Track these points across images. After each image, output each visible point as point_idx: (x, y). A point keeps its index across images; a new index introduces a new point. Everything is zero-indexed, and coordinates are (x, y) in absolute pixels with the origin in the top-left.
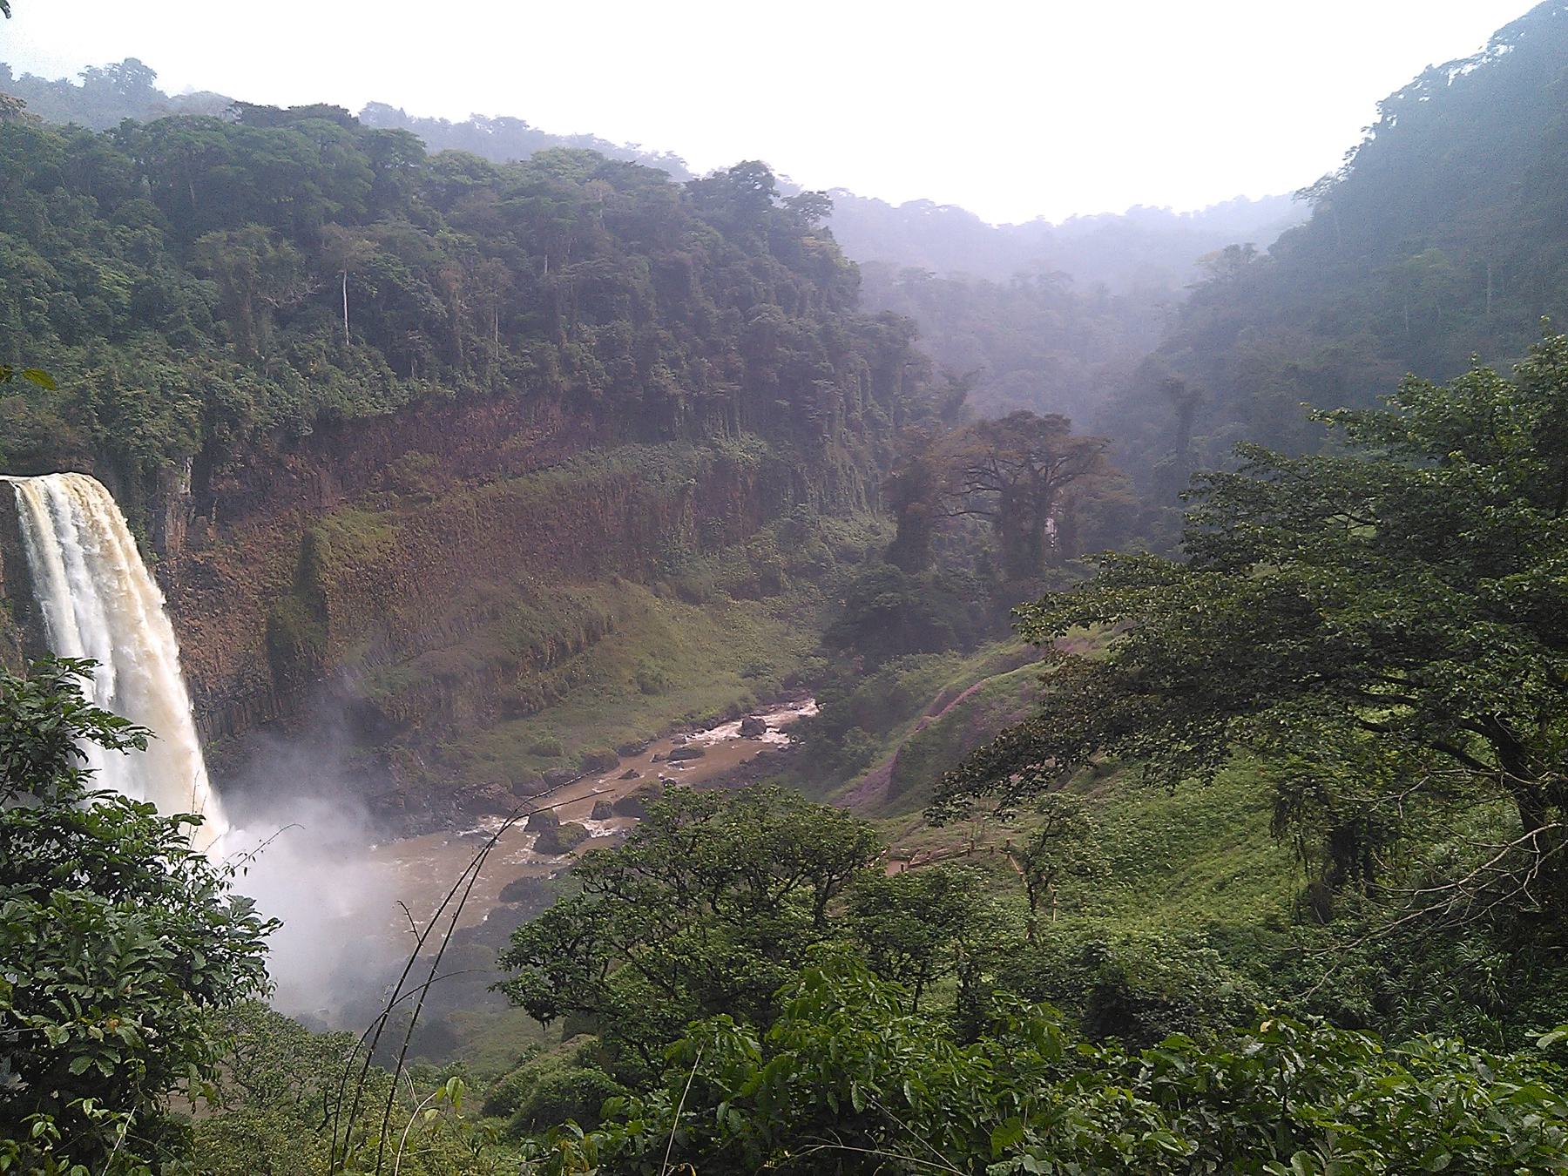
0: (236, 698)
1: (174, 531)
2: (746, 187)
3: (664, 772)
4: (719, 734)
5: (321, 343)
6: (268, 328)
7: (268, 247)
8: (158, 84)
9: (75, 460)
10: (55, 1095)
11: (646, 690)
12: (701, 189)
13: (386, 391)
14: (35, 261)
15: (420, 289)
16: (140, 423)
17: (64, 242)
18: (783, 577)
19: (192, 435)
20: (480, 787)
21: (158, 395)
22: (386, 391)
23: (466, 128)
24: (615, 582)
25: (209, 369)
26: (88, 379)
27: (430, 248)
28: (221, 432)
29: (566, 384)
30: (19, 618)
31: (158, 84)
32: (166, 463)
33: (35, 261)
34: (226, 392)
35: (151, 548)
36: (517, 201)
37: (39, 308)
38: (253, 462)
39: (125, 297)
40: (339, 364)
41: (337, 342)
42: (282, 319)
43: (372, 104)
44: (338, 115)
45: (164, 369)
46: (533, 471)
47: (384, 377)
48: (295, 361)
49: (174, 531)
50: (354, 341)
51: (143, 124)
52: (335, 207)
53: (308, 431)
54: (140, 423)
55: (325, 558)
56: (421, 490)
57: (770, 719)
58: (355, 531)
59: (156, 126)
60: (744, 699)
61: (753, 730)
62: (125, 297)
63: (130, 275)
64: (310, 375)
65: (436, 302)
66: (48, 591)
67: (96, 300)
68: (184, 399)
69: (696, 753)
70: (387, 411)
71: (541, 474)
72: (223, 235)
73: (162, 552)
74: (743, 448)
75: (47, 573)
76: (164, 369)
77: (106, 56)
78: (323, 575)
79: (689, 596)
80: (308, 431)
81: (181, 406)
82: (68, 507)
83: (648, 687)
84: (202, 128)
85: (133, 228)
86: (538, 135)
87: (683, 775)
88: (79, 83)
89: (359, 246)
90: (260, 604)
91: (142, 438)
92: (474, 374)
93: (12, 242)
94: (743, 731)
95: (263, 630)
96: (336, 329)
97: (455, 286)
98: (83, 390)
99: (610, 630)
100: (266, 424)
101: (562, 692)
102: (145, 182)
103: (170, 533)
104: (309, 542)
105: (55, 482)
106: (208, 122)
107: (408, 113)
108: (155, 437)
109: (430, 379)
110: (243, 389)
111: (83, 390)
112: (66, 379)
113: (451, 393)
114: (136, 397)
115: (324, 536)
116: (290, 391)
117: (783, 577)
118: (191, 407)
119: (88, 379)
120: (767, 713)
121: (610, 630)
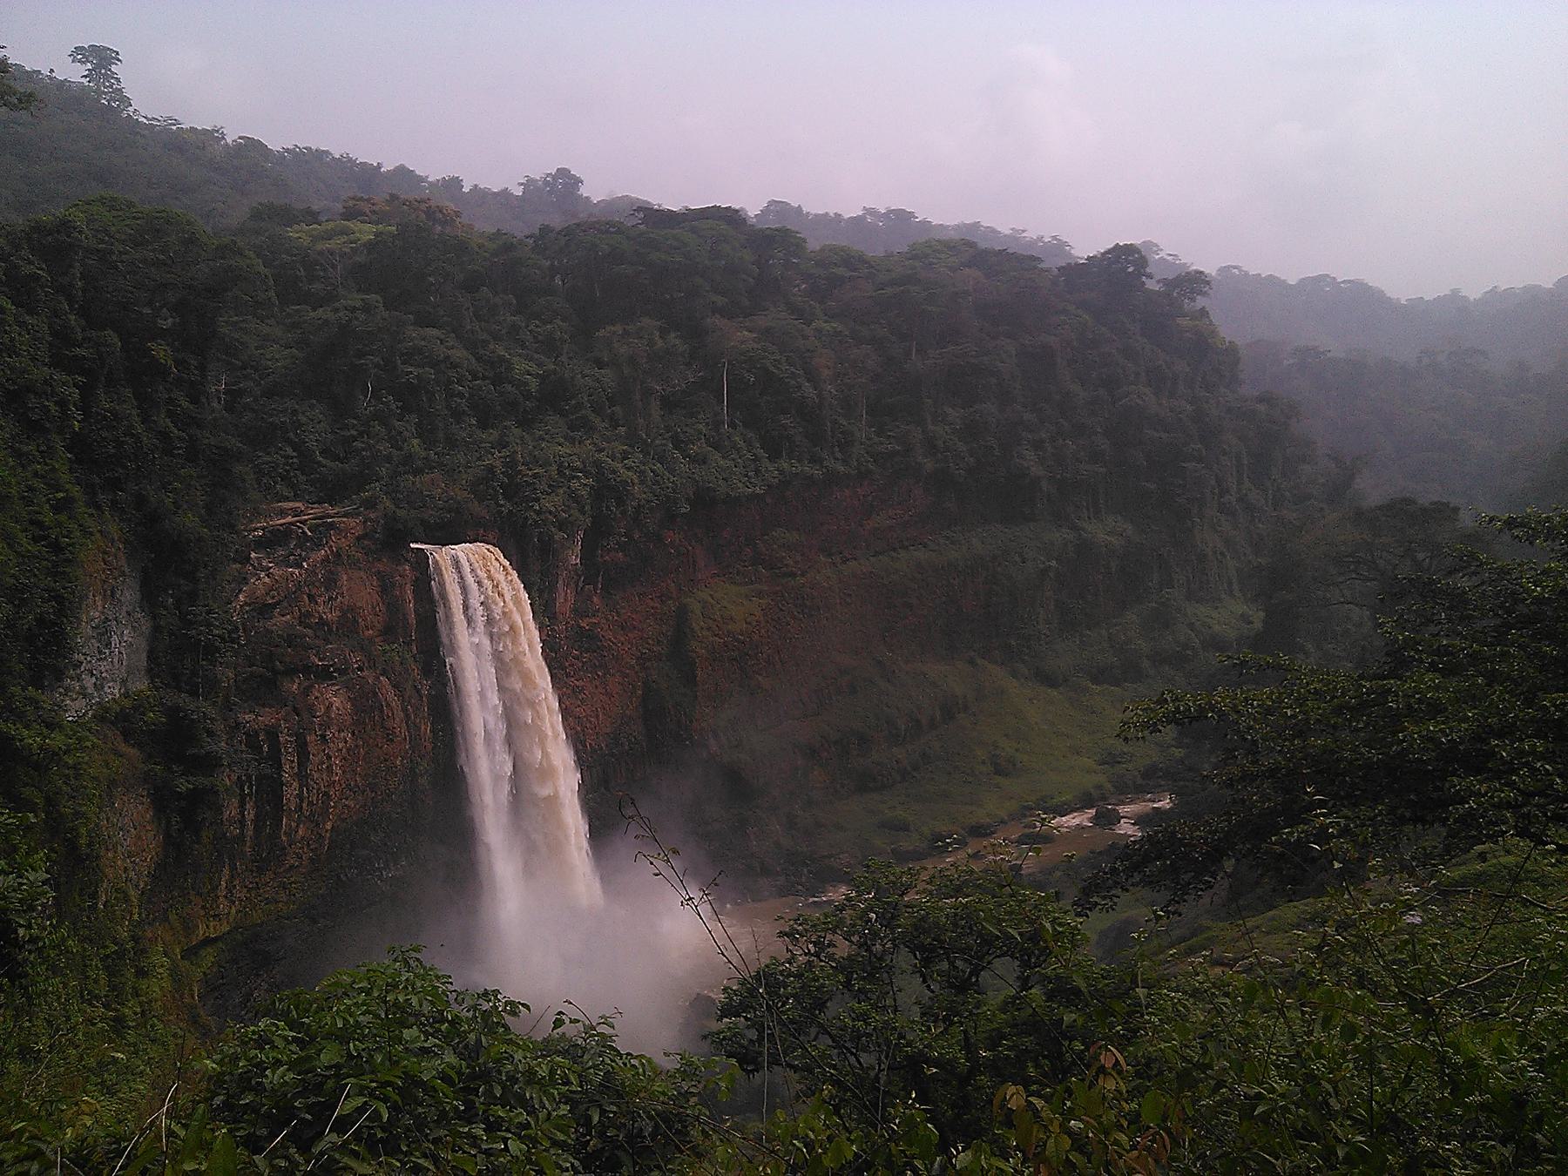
1: (564, 598)
2: (1124, 265)
3: (1010, 856)
4: (1072, 820)
8: (584, 191)
11: (998, 772)
12: (1079, 273)
18: (1146, 663)
24: (972, 662)
29: (929, 465)
30: (427, 671)
46: (894, 550)
49: (564, 598)
57: (1124, 810)
58: (727, 603)
60: (1099, 787)
61: (1107, 819)
66: (453, 650)
69: (1047, 839)
74: (1107, 531)
77: (541, 167)
79: (1050, 680)
87: (1031, 863)
94: (1096, 819)
105: (461, 550)
117: (1146, 663)
120: (1123, 803)
121: (966, 708)
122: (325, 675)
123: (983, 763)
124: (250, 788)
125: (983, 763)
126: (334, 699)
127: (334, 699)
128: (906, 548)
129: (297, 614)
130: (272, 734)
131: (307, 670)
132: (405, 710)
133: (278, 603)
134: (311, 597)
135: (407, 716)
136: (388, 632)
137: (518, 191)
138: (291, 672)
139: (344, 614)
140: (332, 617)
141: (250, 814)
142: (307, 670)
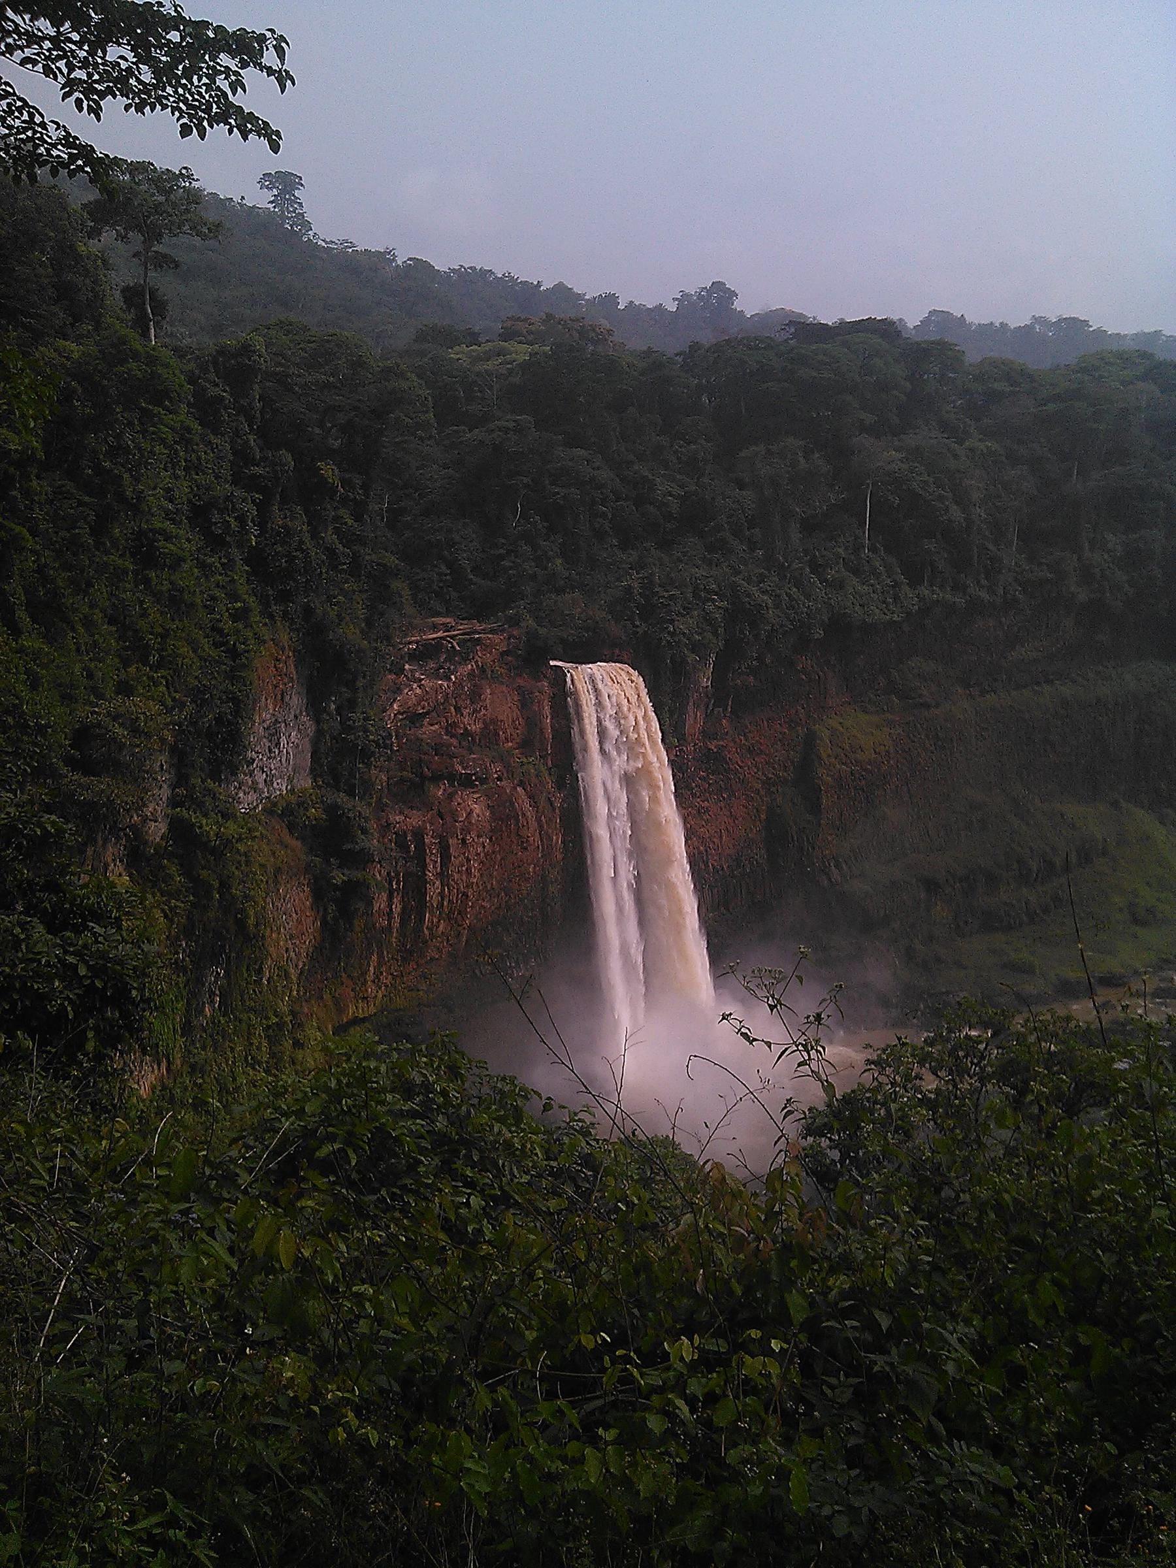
0: (733, 877)
1: (694, 719)
5: (841, 550)
6: (795, 535)
7: (801, 459)
8: (737, 305)
9: (617, 651)
10: (1115, 1523)
11: (1136, 921)
13: (896, 598)
14: (605, 475)
15: (941, 498)
16: (672, 621)
17: (632, 457)
19: (715, 634)
20: (948, 993)
21: (690, 596)
22: (896, 598)
23: (1026, 331)
24: (1115, 804)
25: (737, 573)
26: (634, 581)
27: (956, 456)
28: (741, 632)
29: (1083, 596)
30: (560, 784)
31: (737, 305)
32: (692, 658)
33: (605, 475)
34: (749, 595)
35: (673, 735)
36: (1051, 407)
37: (604, 515)
38: (768, 661)
39: (675, 507)
40: (856, 572)
41: (858, 548)
42: (809, 527)
43: (933, 312)
44: (885, 329)
45: (699, 573)
46: (1038, 684)
47: (896, 585)
48: (816, 568)
49: (694, 719)
50: (873, 549)
51: (707, 346)
52: (869, 418)
53: (819, 633)
54: (672, 621)
55: (824, 756)
56: (920, 696)
58: (855, 731)
59: (717, 348)
62: (675, 507)
63: (682, 487)
64: (826, 581)
65: (956, 513)
67: (651, 508)
68: (713, 601)
70: (896, 618)
71: (1047, 688)
72: (761, 448)
73: (682, 738)
75: (585, 749)
76: (699, 573)
78: (820, 771)
80: (819, 633)
81: (709, 607)
82: (611, 695)
83: (1140, 918)
84: (757, 348)
85: (689, 443)
86: (1100, 333)
88: (672, 307)
89: (885, 456)
90: (762, 792)
91: (672, 634)
92: (984, 582)
93: (589, 457)
95: (763, 816)
96: (856, 538)
97: (976, 496)
98: (628, 589)
99: (1104, 853)
100: (782, 626)
101: (1046, 910)
102: (705, 399)
103: (690, 721)
104: (810, 740)
105: (598, 669)
106: (761, 342)
107: (968, 319)
108: (684, 634)
109: (942, 587)
110: (764, 592)
111: (628, 589)
112: (618, 579)
113: (960, 601)
114: (671, 597)
115: (825, 734)
116: (808, 596)
118: (717, 607)
119: (634, 581)
122: (467, 782)
123: (1121, 910)
124: (398, 884)
125: (1121, 910)
126: (475, 806)
127: (475, 806)
128: (1049, 682)
129: (444, 724)
130: (419, 835)
131: (452, 777)
132: (538, 820)
133: (428, 713)
134: (457, 709)
135: (541, 827)
136: (526, 745)
137: (672, 307)
138: (436, 779)
139: (486, 727)
140: (475, 728)
141: (397, 908)
142: (452, 777)
